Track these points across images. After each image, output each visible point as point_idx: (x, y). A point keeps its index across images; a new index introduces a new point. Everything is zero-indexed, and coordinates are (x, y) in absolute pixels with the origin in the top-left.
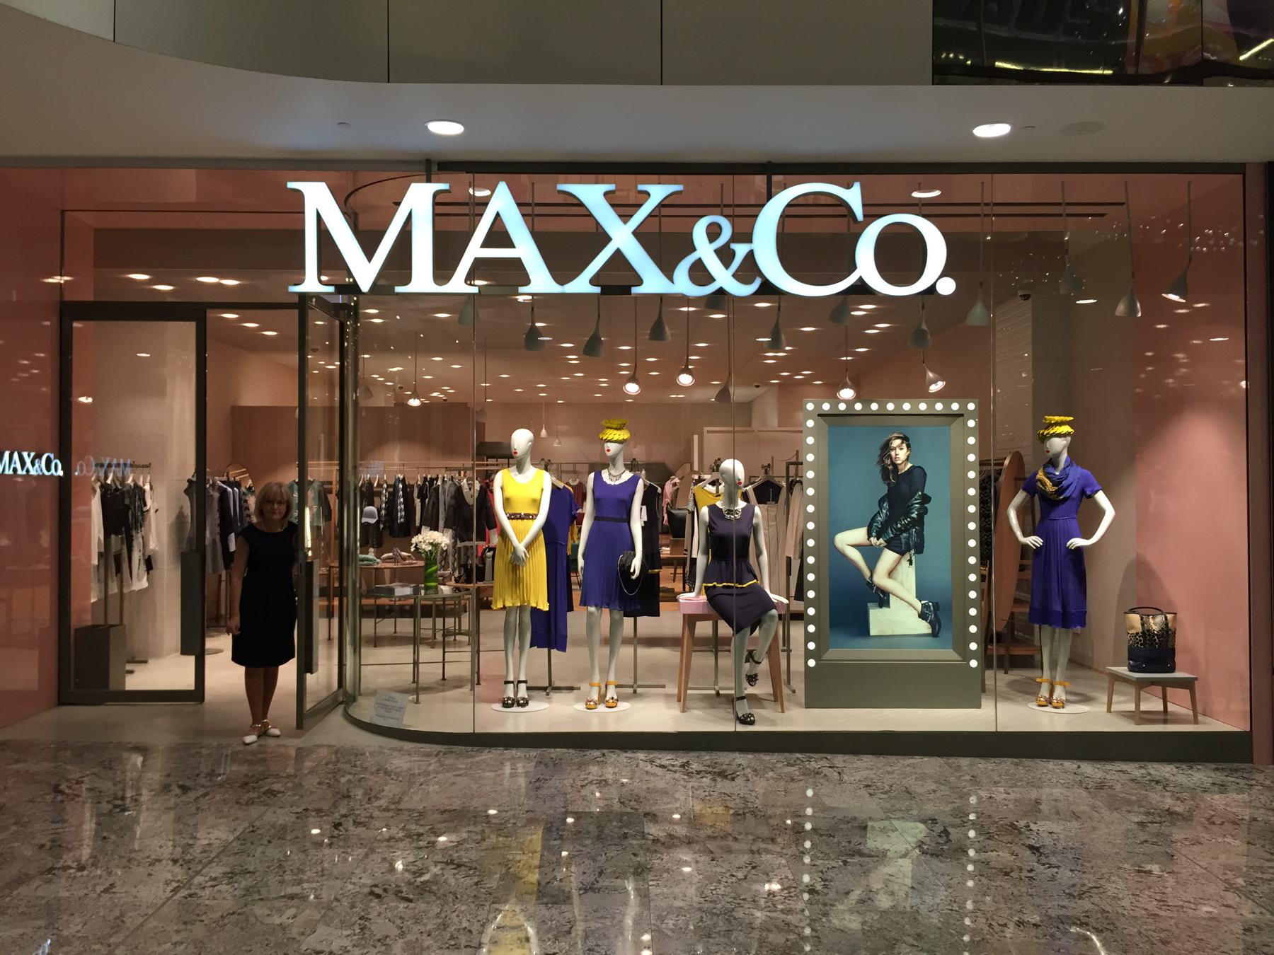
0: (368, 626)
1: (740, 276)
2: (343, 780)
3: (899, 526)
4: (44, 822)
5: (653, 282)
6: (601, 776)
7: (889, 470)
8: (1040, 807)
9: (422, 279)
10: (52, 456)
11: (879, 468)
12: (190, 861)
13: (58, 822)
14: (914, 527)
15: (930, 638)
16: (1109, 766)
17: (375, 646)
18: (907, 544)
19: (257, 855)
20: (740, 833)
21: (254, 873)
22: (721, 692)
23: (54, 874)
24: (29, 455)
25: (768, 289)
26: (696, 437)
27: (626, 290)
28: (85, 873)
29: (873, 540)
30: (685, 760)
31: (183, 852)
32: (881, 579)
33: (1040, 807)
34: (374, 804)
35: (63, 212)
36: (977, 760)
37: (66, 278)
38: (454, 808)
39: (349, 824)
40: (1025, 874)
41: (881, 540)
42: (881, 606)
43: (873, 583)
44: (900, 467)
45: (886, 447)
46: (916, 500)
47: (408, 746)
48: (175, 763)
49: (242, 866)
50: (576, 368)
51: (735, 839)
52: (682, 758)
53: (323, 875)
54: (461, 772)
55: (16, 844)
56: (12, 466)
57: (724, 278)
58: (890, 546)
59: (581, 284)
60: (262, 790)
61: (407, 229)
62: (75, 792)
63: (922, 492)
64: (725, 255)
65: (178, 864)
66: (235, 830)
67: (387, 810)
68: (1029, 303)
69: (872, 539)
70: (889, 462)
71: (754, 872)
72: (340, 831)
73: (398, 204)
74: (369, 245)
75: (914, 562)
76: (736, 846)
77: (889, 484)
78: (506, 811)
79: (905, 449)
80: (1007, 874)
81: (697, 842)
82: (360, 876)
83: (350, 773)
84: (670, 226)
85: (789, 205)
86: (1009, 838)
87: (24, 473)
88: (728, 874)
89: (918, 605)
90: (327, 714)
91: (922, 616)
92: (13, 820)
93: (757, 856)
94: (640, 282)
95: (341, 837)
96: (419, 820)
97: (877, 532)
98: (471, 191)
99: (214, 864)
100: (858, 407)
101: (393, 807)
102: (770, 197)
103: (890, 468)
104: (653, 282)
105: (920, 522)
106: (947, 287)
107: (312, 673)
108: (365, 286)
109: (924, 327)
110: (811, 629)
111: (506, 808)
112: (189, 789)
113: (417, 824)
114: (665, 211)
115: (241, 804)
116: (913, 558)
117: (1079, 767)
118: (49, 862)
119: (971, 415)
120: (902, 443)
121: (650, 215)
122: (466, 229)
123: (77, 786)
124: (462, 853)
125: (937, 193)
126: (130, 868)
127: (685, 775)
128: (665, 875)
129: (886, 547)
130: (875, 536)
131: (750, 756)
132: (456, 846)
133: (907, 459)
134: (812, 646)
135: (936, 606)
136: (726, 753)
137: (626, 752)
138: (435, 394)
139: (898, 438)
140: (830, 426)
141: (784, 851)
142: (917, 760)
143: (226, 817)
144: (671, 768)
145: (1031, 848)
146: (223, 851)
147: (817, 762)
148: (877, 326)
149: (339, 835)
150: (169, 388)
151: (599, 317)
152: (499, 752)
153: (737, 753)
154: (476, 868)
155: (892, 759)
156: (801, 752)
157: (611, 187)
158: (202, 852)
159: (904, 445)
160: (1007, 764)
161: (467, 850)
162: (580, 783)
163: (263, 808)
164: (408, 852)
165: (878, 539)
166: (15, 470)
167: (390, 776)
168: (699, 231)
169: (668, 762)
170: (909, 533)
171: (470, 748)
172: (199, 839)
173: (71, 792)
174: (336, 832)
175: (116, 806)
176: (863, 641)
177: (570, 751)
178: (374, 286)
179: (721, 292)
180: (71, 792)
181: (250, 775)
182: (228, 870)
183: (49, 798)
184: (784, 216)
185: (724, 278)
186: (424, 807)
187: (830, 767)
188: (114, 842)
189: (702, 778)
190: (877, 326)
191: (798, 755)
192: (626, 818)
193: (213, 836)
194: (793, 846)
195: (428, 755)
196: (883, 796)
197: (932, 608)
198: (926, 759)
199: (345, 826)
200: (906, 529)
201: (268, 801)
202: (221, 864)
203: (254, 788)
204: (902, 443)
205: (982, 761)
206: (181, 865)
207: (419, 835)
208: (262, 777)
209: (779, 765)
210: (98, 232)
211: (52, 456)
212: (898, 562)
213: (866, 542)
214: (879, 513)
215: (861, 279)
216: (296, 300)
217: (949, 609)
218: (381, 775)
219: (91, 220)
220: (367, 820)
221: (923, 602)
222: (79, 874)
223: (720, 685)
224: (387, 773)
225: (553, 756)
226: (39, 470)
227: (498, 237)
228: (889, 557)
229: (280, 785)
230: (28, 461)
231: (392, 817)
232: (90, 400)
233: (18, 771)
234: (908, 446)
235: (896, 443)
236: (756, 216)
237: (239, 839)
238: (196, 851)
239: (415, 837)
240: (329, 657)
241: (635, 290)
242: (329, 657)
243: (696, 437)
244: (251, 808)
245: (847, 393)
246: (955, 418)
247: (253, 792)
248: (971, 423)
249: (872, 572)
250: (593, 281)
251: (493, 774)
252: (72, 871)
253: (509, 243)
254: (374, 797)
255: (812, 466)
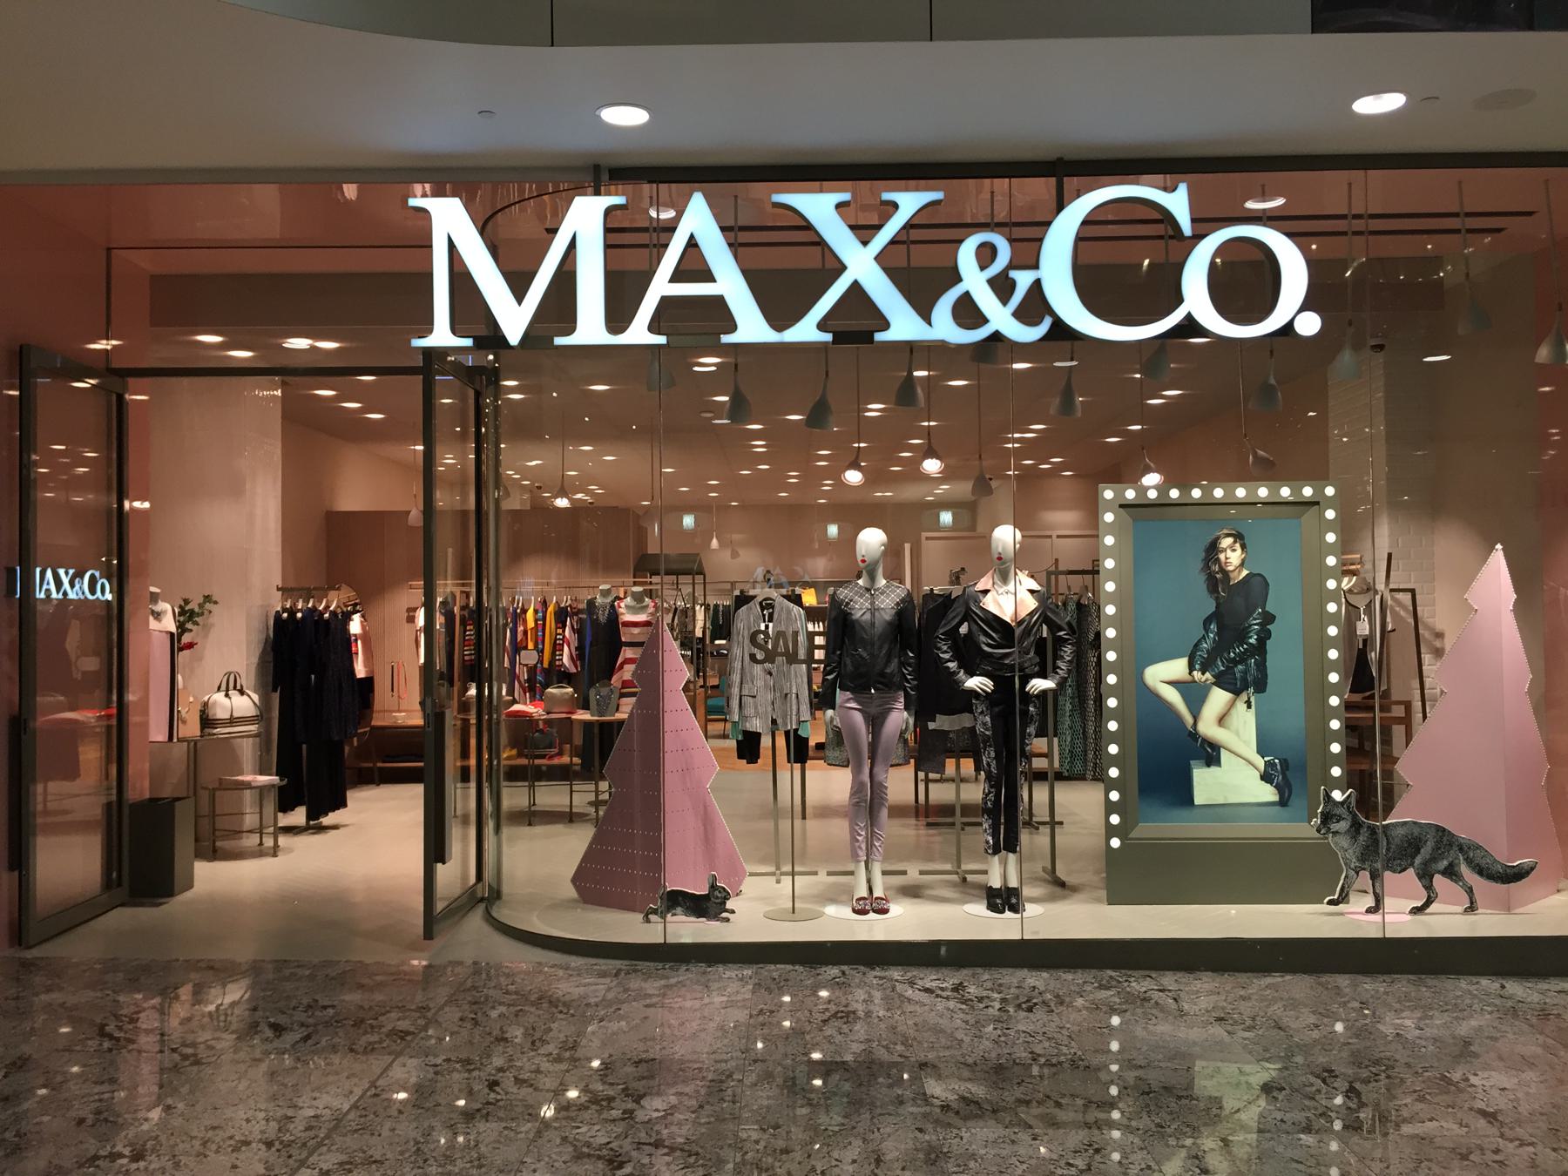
0: (514, 797)
1: (1021, 316)
2: (494, 1014)
3: (1232, 655)
4: (84, 1083)
5: (903, 325)
6: (846, 1006)
7: (1216, 579)
8: (1472, 1048)
9: (590, 328)
10: (97, 574)
11: (1203, 577)
12: (289, 1144)
13: (103, 1083)
14: (1252, 656)
15: (1278, 808)
16: (1543, 986)
17: (530, 824)
18: (1244, 679)
19: (386, 1133)
20: (1064, 1096)
21: (381, 1162)
22: (970, 877)
23: (98, 1166)
24: (67, 573)
25: (1061, 331)
26: (907, 546)
27: (867, 337)
28: (142, 1164)
29: (1197, 675)
30: (956, 982)
31: (280, 1130)
32: (1208, 727)
33: (1472, 1048)
34: (541, 1051)
35: (109, 250)
36: (1360, 978)
37: (115, 342)
38: (652, 1056)
39: (508, 1081)
40: (1490, 1156)
41: (1208, 675)
42: (1208, 765)
43: (1197, 733)
44: (1232, 575)
45: (1213, 548)
46: (1255, 619)
47: (576, 961)
48: (263, 990)
49: (364, 1152)
50: (761, 458)
51: (1058, 1105)
52: (951, 979)
53: (480, 1167)
54: (655, 1000)
55: (46, 1119)
56: (45, 587)
57: (1001, 318)
58: (1221, 682)
59: (806, 330)
60: (383, 1030)
61: (565, 268)
62: (127, 1036)
63: (1263, 608)
64: (1002, 287)
65: (273, 1149)
66: (351, 1092)
67: (559, 1060)
68: (1380, 358)
69: (1195, 673)
70: (1217, 568)
71: (1098, 1157)
72: (498, 1093)
73: (554, 231)
74: (519, 285)
75: (1253, 704)
76: (1062, 1116)
77: (1217, 599)
78: (726, 1061)
79: (1239, 551)
80: (1464, 1157)
81: (1005, 1109)
82: (533, 1167)
83: (501, 1004)
84: (923, 257)
85: (1085, 223)
86: (1447, 1099)
87: (60, 596)
88: (1062, 1163)
89: (1260, 763)
90: (464, 916)
91: (1266, 777)
92: (41, 1081)
93: (1096, 1132)
94: (885, 325)
95: (501, 1103)
96: (606, 1076)
97: (1202, 663)
98: (653, 214)
99: (325, 1149)
100: (1174, 494)
101: (567, 1054)
102: (1060, 207)
103: (1218, 576)
104: (903, 325)
105: (1261, 649)
106: (1309, 325)
107: (444, 863)
108: (514, 334)
109: (1272, 381)
110: (1114, 796)
111: (725, 1057)
112: (285, 1029)
113: (604, 1083)
114: (915, 234)
115: (357, 1053)
116: (1252, 699)
117: (1503, 987)
118: (91, 1146)
119: (1331, 503)
120: (1235, 542)
121: (893, 242)
122: (646, 267)
123: (131, 1027)
124: (674, 1129)
125: (1279, 201)
126: (205, 1156)
127: (962, 1003)
128: (972, 1164)
129: (1214, 684)
130: (1200, 670)
131: (1045, 975)
132: (664, 1117)
133: (1242, 564)
134: (1115, 819)
135: (1284, 763)
136: (1011, 970)
137: (873, 969)
138: (579, 496)
139: (1228, 535)
140: (1134, 520)
141: (1134, 1123)
142: (1275, 979)
143: (337, 1073)
144: (940, 992)
145: (1484, 1113)
146: (336, 1128)
147: (1140, 984)
148: (1164, 393)
149: (498, 1101)
150: (248, 486)
151: (827, 375)
152: (701, 970)
153: (1026, 970)
154: (697, 1154)
155: (1242, 978)
156: (1114, 968)
157: (846, 197)
158: (307, 1129)
159: (1238, 546)
160: (1403, 985)
161: (680, 1124)
162: (820, 1017)
163: (389, 1059)
164: (597, 1127)
165: (1203, 674)
166: (48, 591)
167: (557, 1007)
168: (966, 255)
169: (934, 984)
170: (1246, 665)
171: (660, 965)
172: (301, 1108)
173: (122, 1035)
174: (492, 1095)
175: (185, 1057)
176: (1184, 813)
177: (797, 967)
178: (526, 337)
179: (997, 337)
180: (122, 1035)
181: (366, 1007)
182: (344, 1158)
183: (92, 1044)
184: (1079, 239)
185: (1001, 318)
186: (611, 1056)
187: (1160, 990)
188: (182, 1114)
189: (987, 1007)
190: (1164, 393)
191: (1110, 972)
192: (895, 1070)
193: (320, 1104)
194: (1144, 1115)
195: (603, 975)
196: (1247, 1034)
197: (1279, 767)
198: (1288, 977)
199: (502, 1085)
200: (1242, 659)
201: (394, 1047)
202: (334, 1148)
203: (372, 1027)
204: (1235, 542)
205: (1368, 980)
206: (278, 1150)
207: (611, 1099)
208: (383, 1011)
209: (1088, 988)
210: (156, 280)
211: (97, 574)
212: (1232, 705)
213: (1186, 677)
214: (1204, 637)
215: (1189, 317)
216: (419, 361)
217: (1303, 768)
218: (545, 1005)
219: (146, 262)
220: (533, 1076)
221: (1267, 759)
222: (134, 1166)
223: (964, 867)
224: (554, 1003)
225: (775, 975)
226: (80, 593)
227: (693, 267)
228: (1219, 698)
229: (407, 1022)
230: (66, 580)
231: (568, 1071)
232: (147, 505)
233: (50, 1004)
234: (1243, 547)
235: (1226, 542)
236: (1041, 240)
237: (357, 1108)
238: (297, 1128)
239: (604, 1103)
240: (465, 838)
241: (880, 337)
242: (465, 838)
243: (907, 546)
244: (371, 1057)
245: (1152, 479)
246: (1307, 508)
247: (372, 1032)
248: (1330, 514)
249: (1196, 718)
250: (822, 326)
251: (697, 1004)
252: (125, 1161)
253: (707, 276)
254: (540, 1039)
255: (1112, 575)
